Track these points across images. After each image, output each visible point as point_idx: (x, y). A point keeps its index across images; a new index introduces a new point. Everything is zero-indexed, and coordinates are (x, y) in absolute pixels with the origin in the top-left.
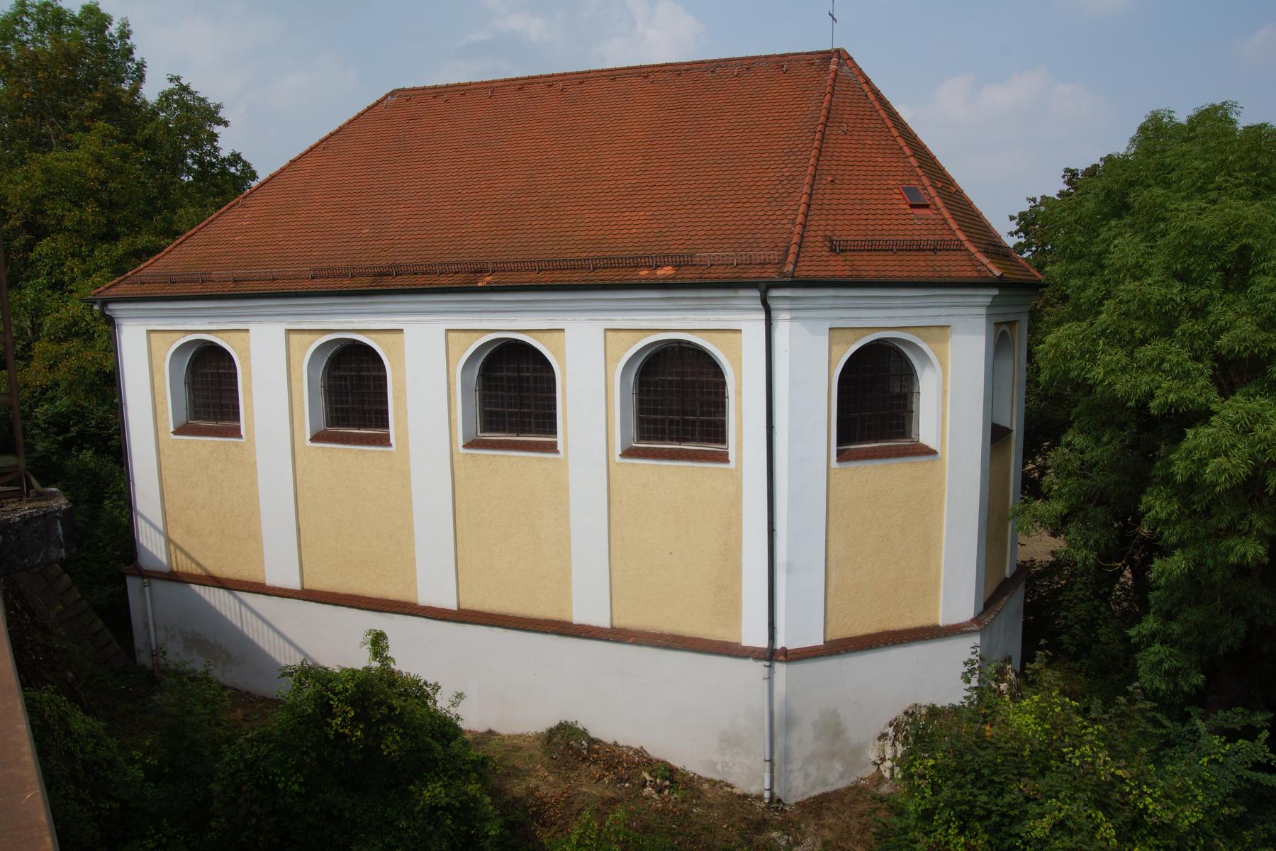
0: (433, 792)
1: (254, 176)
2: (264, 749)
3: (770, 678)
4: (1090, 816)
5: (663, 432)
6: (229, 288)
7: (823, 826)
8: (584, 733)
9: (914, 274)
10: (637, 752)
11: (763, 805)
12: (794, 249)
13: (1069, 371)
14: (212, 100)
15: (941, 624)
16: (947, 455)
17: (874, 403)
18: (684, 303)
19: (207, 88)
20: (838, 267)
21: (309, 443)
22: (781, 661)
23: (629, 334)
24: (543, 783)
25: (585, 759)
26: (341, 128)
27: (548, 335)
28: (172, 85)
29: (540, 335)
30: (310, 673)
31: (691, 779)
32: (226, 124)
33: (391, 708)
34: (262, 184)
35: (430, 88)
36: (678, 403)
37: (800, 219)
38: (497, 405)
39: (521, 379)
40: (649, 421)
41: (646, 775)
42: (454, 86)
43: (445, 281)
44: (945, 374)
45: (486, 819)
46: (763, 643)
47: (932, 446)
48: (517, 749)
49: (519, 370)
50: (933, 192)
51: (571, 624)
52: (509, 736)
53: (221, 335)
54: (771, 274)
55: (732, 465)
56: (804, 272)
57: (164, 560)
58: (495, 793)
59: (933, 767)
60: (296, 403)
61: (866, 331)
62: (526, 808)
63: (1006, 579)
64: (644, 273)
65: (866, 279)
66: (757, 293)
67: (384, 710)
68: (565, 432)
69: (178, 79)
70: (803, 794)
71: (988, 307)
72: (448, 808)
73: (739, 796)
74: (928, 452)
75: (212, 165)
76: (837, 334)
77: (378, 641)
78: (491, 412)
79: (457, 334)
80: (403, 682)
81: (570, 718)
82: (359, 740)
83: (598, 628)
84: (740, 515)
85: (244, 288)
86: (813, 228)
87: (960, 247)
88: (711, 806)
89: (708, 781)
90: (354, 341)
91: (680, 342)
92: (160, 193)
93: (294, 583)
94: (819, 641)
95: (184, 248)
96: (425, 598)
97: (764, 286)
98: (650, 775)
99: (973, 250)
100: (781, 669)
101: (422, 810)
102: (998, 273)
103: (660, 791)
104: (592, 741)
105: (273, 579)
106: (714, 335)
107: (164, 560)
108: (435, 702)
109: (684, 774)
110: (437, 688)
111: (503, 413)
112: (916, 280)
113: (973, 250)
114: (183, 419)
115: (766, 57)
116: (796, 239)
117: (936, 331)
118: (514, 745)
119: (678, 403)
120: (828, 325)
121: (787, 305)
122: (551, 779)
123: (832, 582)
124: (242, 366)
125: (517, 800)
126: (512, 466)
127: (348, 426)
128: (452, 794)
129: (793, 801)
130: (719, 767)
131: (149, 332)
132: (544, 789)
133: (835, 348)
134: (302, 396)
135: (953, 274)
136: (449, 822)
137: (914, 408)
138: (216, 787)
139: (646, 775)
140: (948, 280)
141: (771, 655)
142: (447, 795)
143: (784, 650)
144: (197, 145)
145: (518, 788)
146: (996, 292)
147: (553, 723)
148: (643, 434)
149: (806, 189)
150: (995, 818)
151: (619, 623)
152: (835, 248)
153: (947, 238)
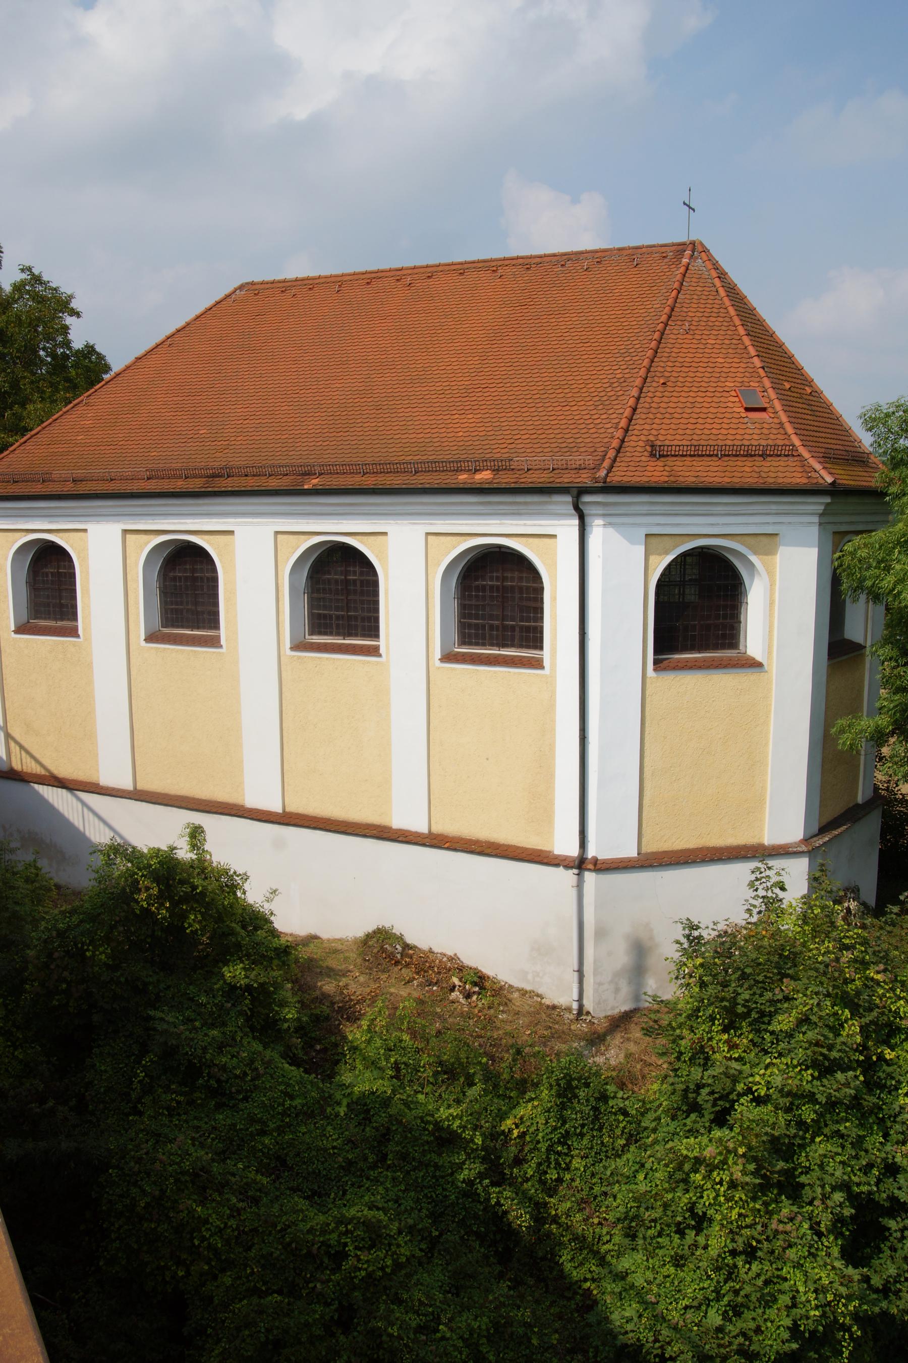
0: (235, 972)
1: (107, 368)
2: (75, 919)
3: (580, 886)
4: (836, 1014)
5: (484, 638)
6: (69, 488)
7: (628, 1039)
8: (400, 938)
9: (736, 480)
10: (451, 959)
11: (572, 1017)
12: (611, 454)
13: (864, 580)
14: (66, 289)
15: (766, 842)
16: (773, 667)
17: (696, 611)
18: (501, 507)
19: (59, 278)
20: (656, 473)
21: (143, 643)
22: (589, 870)
23: (449, 538)
24: (357, 985)
25: (397, 963)
26: (188, 324)
27: (372, 538)
28: (24, 276)
29: (365, 538)
30: (118, 850)
31: (501, 988)
32: (78, 314)
33: (194, 888)
34: (118, 375)
35: (279, 282)
36: (496, 605)
37: (623, 423)
38: (325, 608)
39: (347, 582)
40: (470, 626)
41: (456, 980)
42: (303, 280)
43: (274, 483)
44: (772, 585)
45: (283, 1004)
46: (573, 851)
47: (759, 657)
48: (336, 951)
49: (347, 573)
50: (772, 394)
51: (390, 828)
52: (328, 940)
53: (61, 534)
54: (585, 479)
55: (547, 671)
56: (616, 478)
57: (4, 757)
58: (301, 987)
59: (702, 965)
60: (131, 602)
61: (686, 538)
62: (333, 1003)
63: (857, 805)
64: (463, 477)
65: (683, 485)
66: (568, 499)
67: (187, 889)
68: (387, 636)
69: (29, 269)
70: (613, 1008)
71: (821, 515)
72: (248, 988)
73: (548, 1007)
74: (755, 665)
75: (65, 357)
76: (653, 540)
77: (196, 834)
78: (319, 615)
79: (286, 536)
80: (213, 869)
81: (387, 925)
82: (164, 918)
83: (416, 833)
84: (553, 721)
85: (82, 488)
86: (636, 432)
87: (791, 453)
88: (517, 1013)
89: (519, 990)
90: (189, 542)
91: (500, 547)
92: (11, 387)
93: (127, 784)
94: (633, 853)
95: (28, 446)
96: (251, 801)
97: (575, 492)
98: (460, 980)
99: (806, 455)
100: (590, 877)
101: (221, 989)
102: (829, 479)
103: (468, 996)
104: (407, 946)
105: (106, 779)
106: (531, 540)
107: (4, 757)
108: (244, 893)
109: (495, 981)
110: (245, 877)
111: (331, 617)
112: (738, 486)
113: (806, 455)
114: (24, 618)
115: (620, 249)
116: (615, 443)
117: (764, 540)
118: (334, 949)
119: (496, 605)
120: (643, 531)
121: (600, 511)
122: (362, 979)
123: (648, 794)
124: (81, 565)
125: (325, 996)
126: (338, 668)
127: (182, 627)
128: (252, 976)
129: (602, 1015)
130: (530, 977)
131: (125, 532)
132: (353, 987)
133: (653, 559)
134: (137, 597)
135: (780, 480)
136: (247, 1002)
137: (742, 619)
138: (31, 953)
139: (456, 980)
140: (773, 486)
141: (581, 864)
142: (246, 977)
143: (595, 861)
144: (49, 338)
145: (328, 986)
146: (828, 500)
147: (370, 928)
148: (465, 640)
149: (635, 392)
150: (754, 1015)
151: (437, 829)
152: (657, 452)
153: (780, 443)
